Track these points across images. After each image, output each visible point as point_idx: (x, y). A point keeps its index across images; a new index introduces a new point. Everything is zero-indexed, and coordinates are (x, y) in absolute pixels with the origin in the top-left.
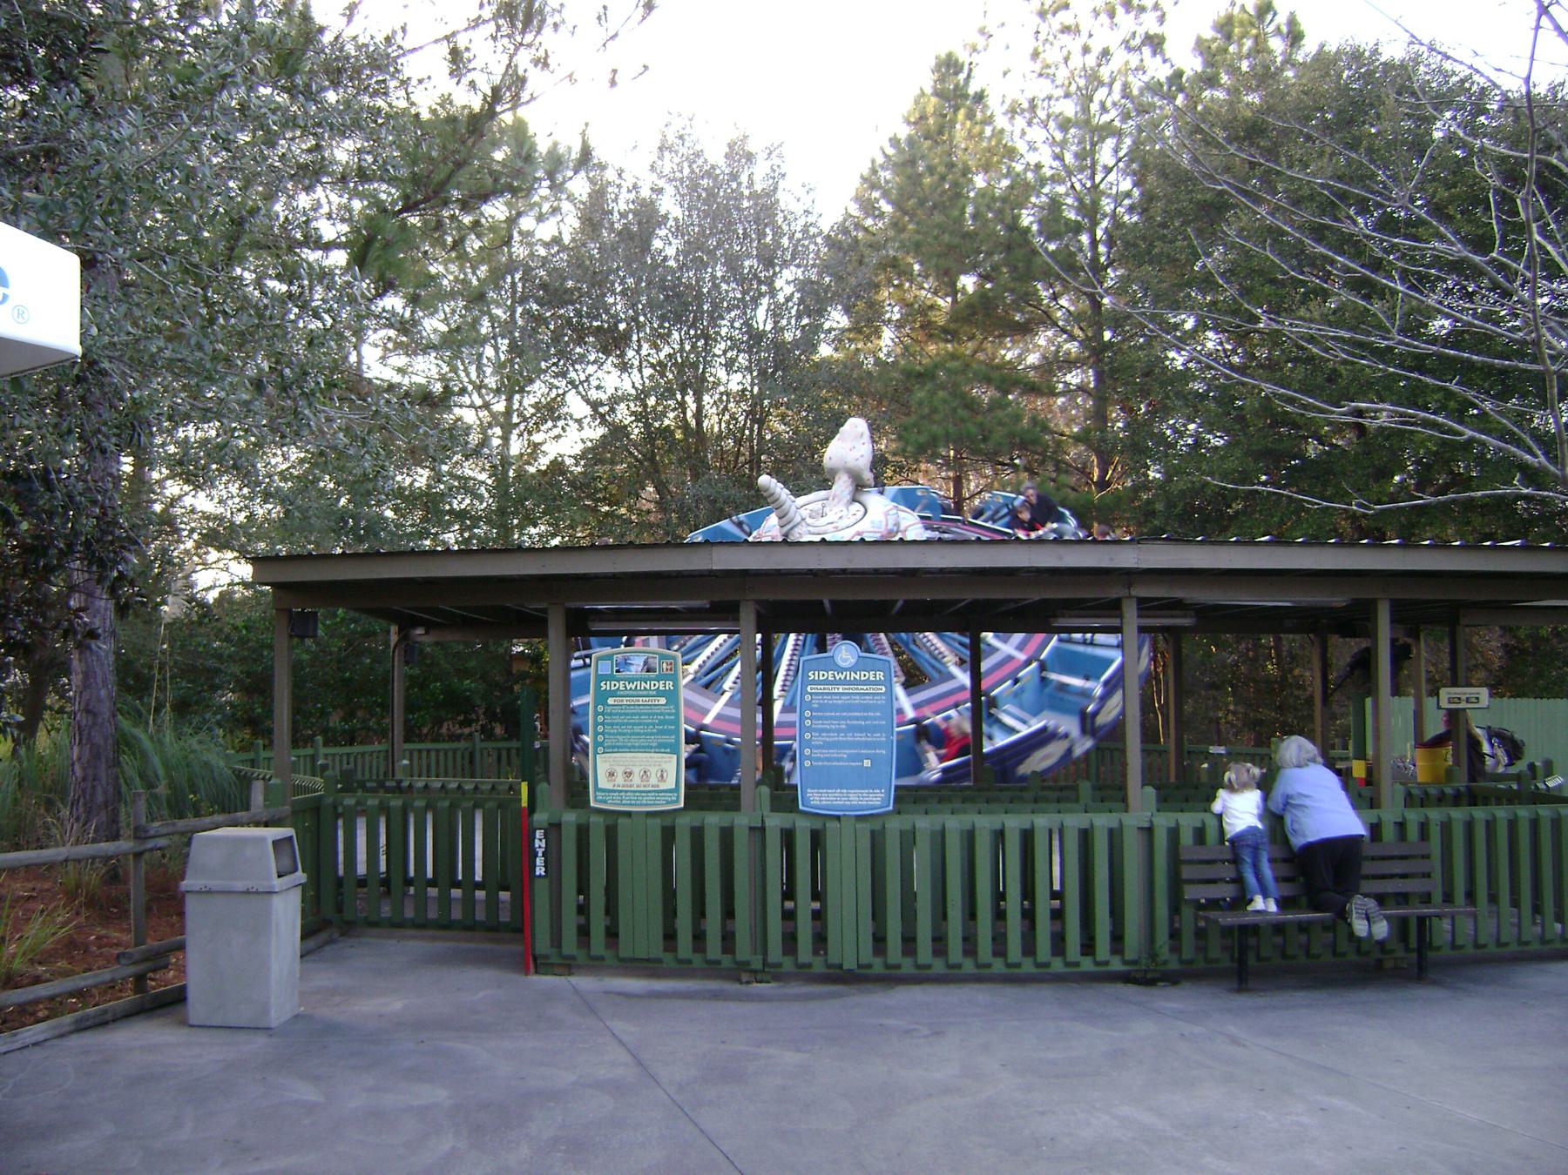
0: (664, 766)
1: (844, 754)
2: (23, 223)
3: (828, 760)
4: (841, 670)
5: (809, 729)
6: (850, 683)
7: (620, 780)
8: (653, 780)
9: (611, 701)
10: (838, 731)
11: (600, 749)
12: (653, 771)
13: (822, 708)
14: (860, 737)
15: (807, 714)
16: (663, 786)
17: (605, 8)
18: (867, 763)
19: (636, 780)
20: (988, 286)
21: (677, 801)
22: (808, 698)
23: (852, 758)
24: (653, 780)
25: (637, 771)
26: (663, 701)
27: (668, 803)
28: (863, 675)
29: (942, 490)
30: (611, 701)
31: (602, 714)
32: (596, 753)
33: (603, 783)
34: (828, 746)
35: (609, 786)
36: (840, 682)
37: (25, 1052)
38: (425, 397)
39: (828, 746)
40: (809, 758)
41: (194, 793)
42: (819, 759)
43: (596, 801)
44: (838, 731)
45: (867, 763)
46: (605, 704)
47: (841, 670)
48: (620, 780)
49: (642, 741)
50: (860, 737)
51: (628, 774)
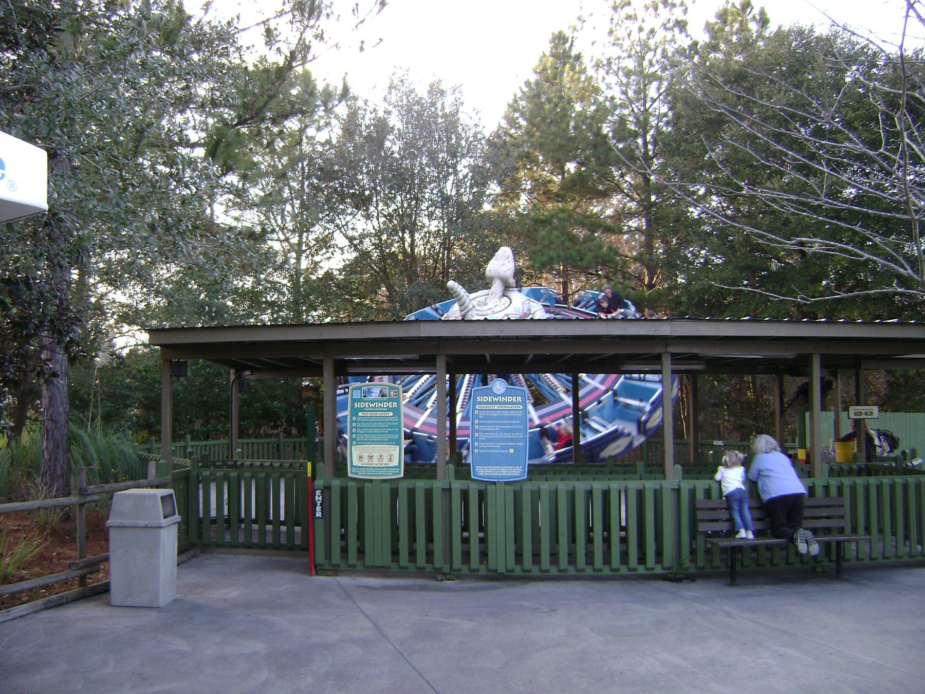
0: (392, 453)
1: (498, 445)
2: (14, 132)
3: (489, 449)
4: (496, 396)
5: (477, 431)
6: (501, 403)
7: (366, 460)
8: (385, 461)
9: (360, 414)
10: (495, 432)
11: (354, 442)
12: (385, 455)
13: (485, 418)
14: (507, 435)
15: (476, 421)
16: (391, 464)
17: (357, 5)
18: (512, 451)
19: (375, 461)
20: (583, 169)
21: (400, 473)
22: (476, 412)
23: (502, 448)
24: (385, 461)
25: (376, 455)
26: (391, 414)
27: (394, 474)
28: (509, 399)
29: (556, 290)
30: (360, 414)
31: (355, 422)
32: (352, 445)
33: (356, 462)
34: (488, 440)
35: (359, 464)
36: (496, 403)
37: (15, 621)
38: (251, 235)
39: (488, 440)
40: (477, 448)
41: (115, 468)
42: (483, 448)
43: (352, 473)
44: (495, 432)
45: (512, 451)
46: (357, 416)
47: (496, 396)
48: (366, 460)
49: (379, 438)
50: (507, 435)
51: (371, 457)
